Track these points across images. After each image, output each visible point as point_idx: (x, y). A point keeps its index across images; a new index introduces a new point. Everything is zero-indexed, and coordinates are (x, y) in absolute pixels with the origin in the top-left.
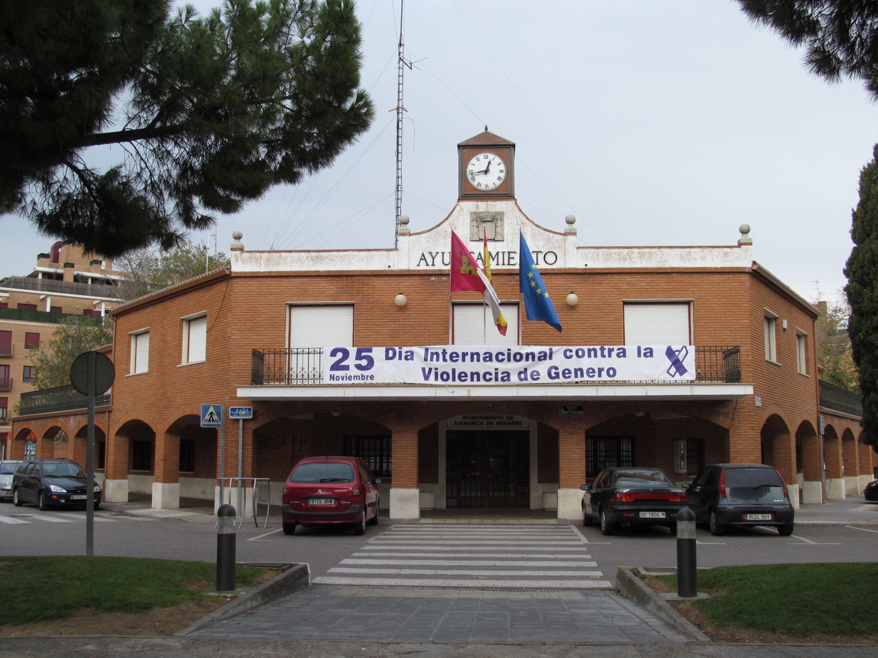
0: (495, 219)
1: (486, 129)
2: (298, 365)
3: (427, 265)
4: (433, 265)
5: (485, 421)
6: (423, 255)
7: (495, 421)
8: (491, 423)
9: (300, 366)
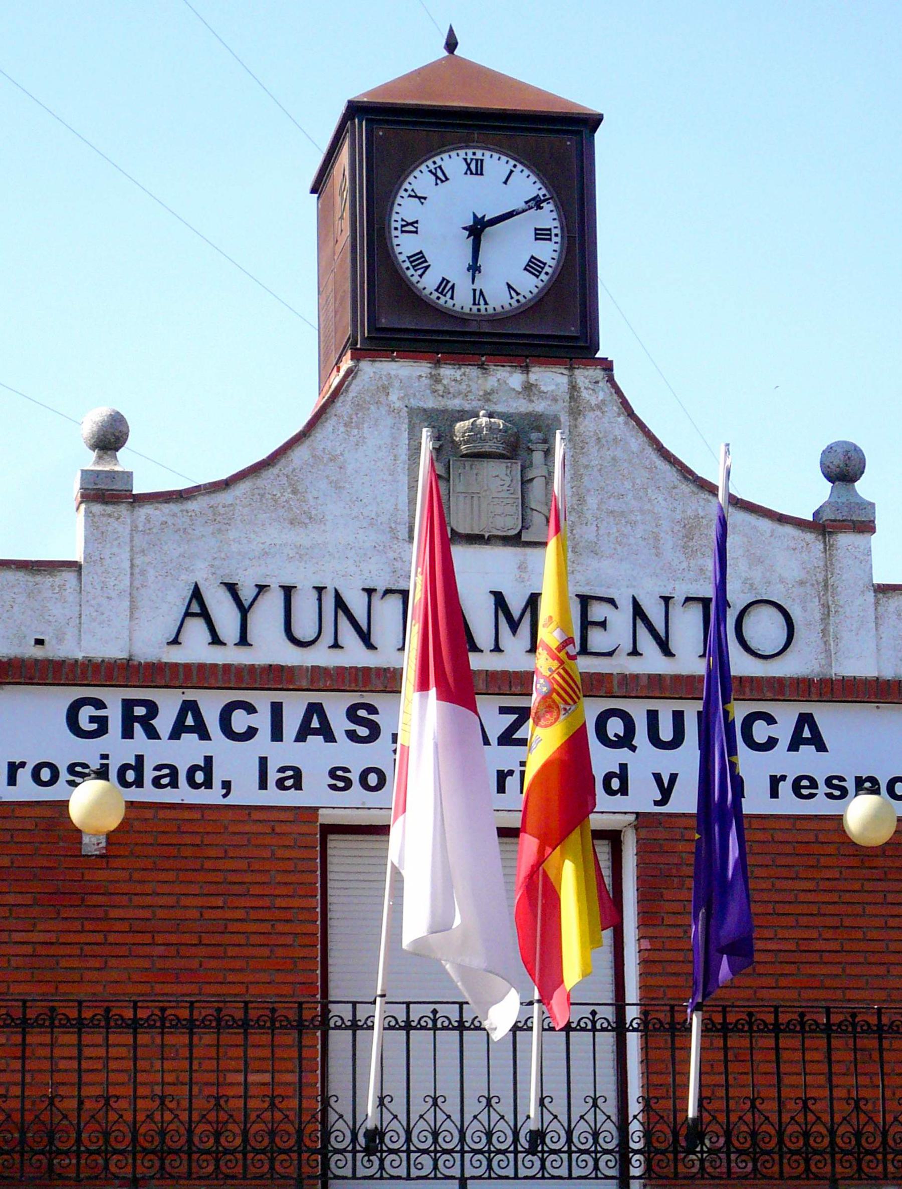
0: (520, 443)
1: (451, 44)
3: (216, 640)
4: (243, 641)
6: (197, 594)
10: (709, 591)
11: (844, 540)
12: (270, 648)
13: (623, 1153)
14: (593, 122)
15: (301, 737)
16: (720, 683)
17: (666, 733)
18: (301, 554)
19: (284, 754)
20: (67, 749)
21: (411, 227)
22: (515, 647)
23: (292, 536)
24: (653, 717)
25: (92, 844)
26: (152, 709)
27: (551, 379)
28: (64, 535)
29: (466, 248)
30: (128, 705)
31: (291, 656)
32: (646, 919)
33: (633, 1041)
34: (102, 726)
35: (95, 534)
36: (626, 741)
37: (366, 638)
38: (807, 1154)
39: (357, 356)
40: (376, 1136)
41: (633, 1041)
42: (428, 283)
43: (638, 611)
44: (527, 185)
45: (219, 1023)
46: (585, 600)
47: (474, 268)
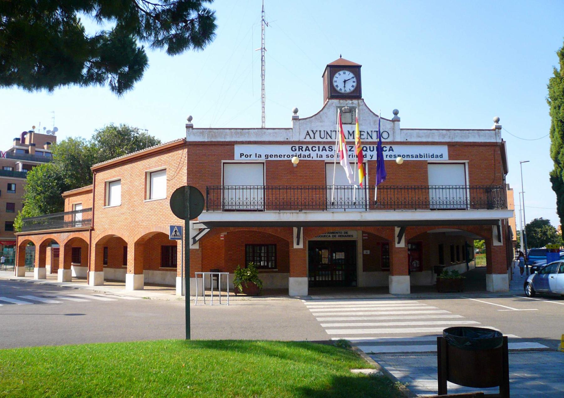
0: (351, 110)
1: (341, 57)
2: (231, 197)
4: (314, 138)
5: (331, 235)
6: (308, 132)
7: (337, 235)
8: (335, 236)
9: (346, 197)
10: (378, 130)
11: (396, 123)
12: (318, 139)
13: (366, 205)
14: (361, 66)
15: (322, 150)
16: (380, 143)
17: (372, 149)
18: (322, 126)
19: (320, 153)
20: (292, 153)
21: (336, 81)
22: (351, 138)
23: (320, 124)
24: (370, 147)
25: (295, 165)
26: (302, 147)
27: (355, 102)
28: (290, 124)
29: (343, 83)
30: (299, 147)
31: (321, 140)
32: (369, 174)
33: (367, 190)
34: (296, 150)
35: (294, 124)
36: (366, 150)
37: (331, 137)
38: (391, 205)
39: (329, 99)
40: (333, 203)
41: (367, 190)
42: (338, 89)
43: (368, 133)
44: (352, 75)
45: (312, 189)
46: (360, 132)
47: (345, 87)
